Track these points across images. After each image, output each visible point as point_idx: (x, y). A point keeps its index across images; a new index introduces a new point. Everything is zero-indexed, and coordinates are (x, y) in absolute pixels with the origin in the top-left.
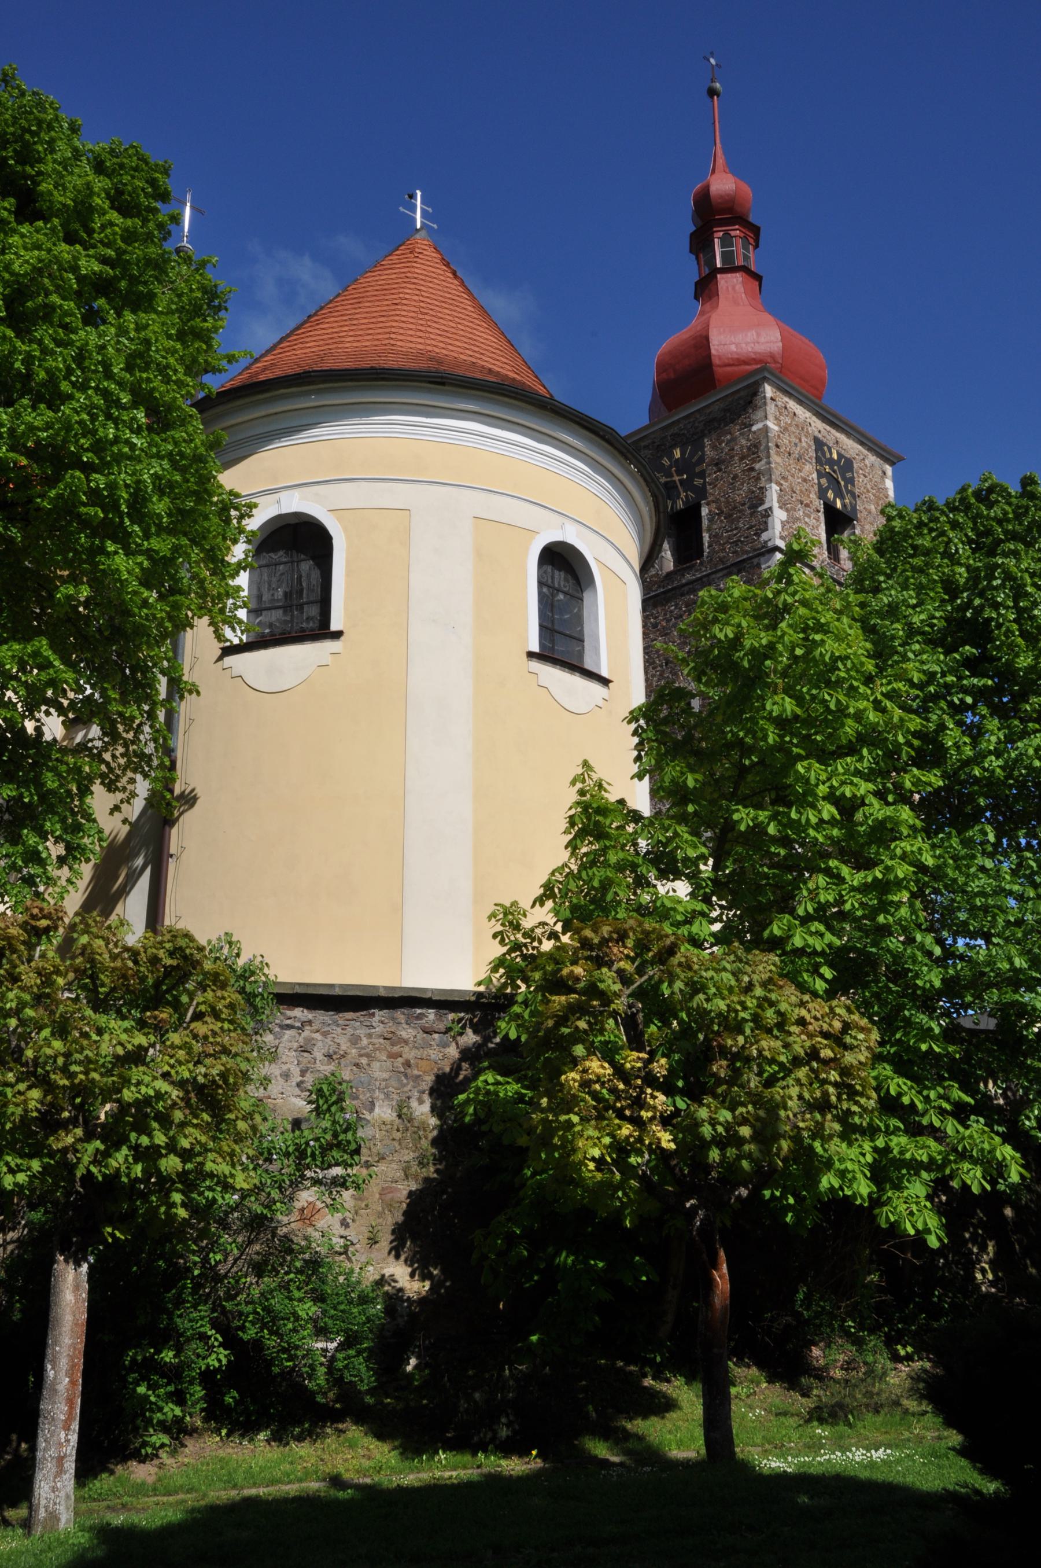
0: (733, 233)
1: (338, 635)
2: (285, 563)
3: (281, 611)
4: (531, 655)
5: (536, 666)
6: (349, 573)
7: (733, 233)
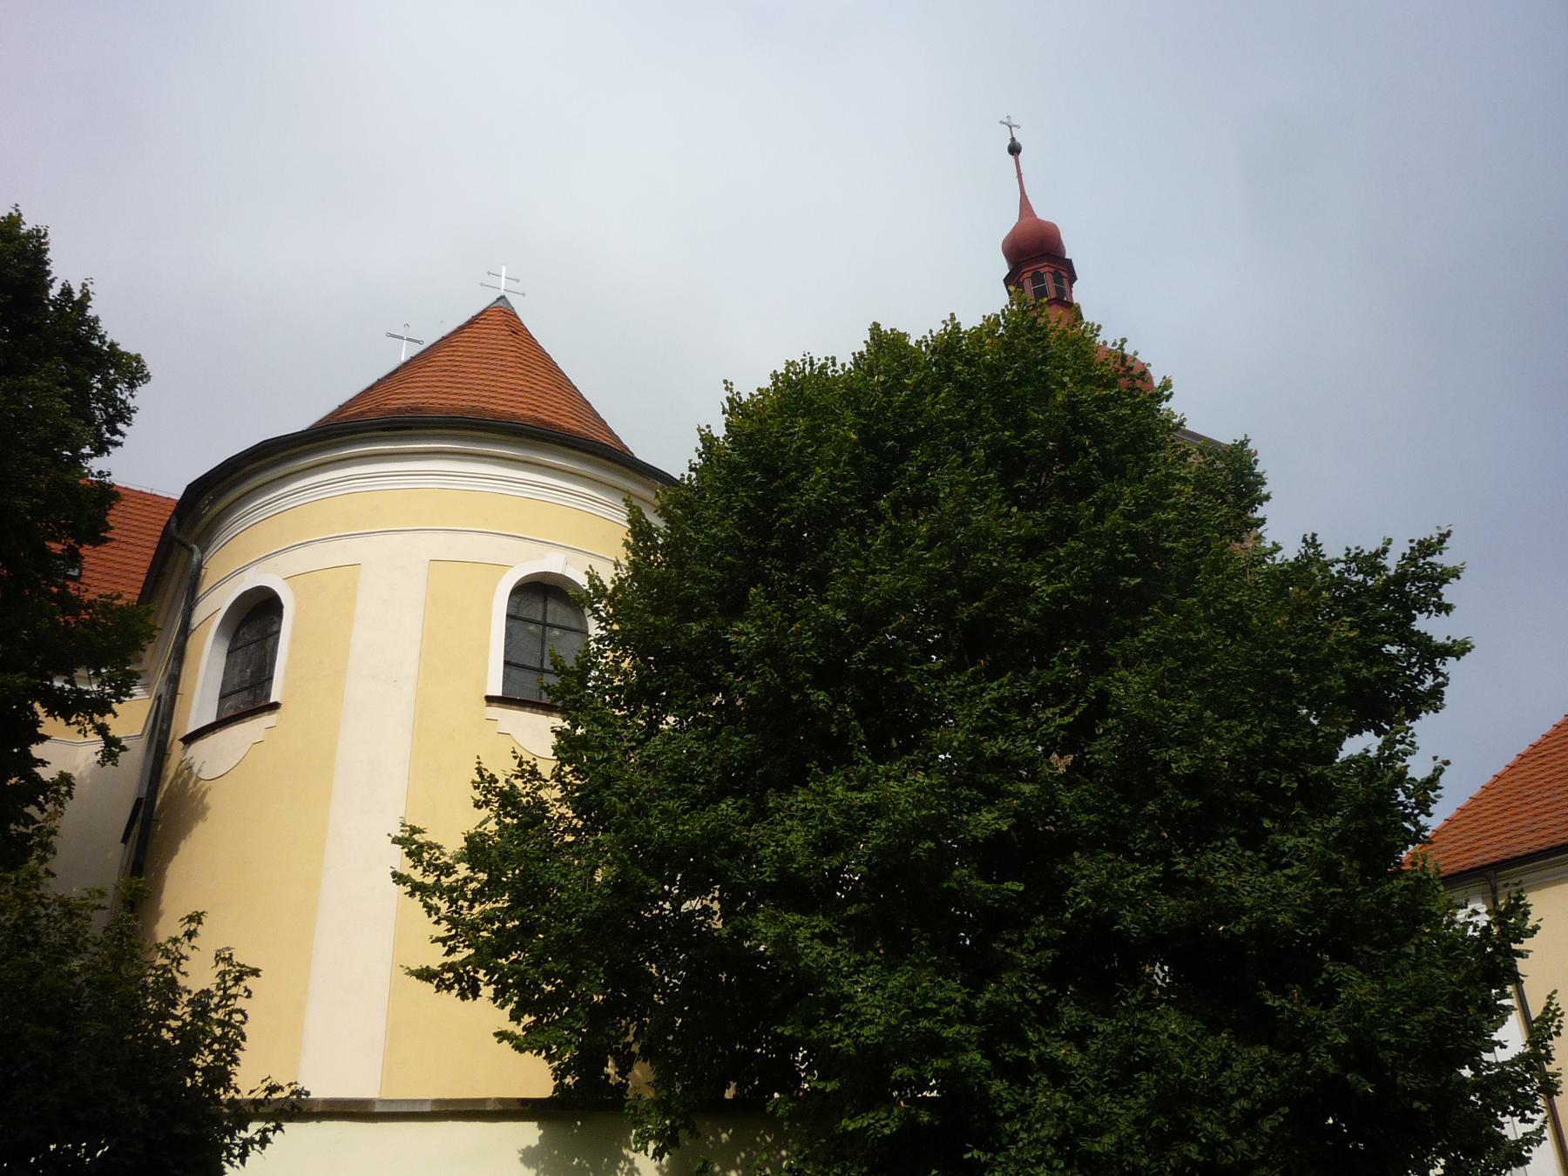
0: (1042, 271)
1: (276, 706)
2: (254, 642)
3: (246, 693)
4: (490, 700)
5: (496, 711)
6: (293, 641)
7: (1042, 271)
